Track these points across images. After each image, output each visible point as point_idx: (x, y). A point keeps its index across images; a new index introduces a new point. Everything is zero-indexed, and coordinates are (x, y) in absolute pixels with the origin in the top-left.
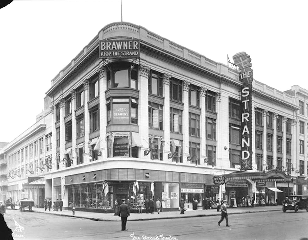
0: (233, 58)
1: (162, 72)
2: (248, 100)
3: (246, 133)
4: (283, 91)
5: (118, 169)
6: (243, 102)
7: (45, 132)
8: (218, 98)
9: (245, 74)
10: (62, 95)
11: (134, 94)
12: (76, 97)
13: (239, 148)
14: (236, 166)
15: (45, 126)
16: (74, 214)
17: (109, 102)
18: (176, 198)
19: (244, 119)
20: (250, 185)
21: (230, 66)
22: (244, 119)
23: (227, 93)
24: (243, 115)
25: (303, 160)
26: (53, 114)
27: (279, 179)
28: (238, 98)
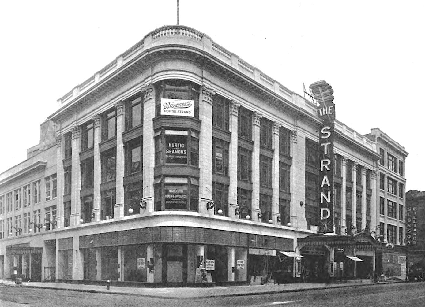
0: (310, 88)
1: (229, 99)
2: (330, 143)
3: (325, 185)
4: (362, 134)
5: (171, 228)
6: (322, 145)
7: (44, 173)
8: (293, 138)
9: (325, 109)
10: (77, 120)
11: (194, 126)
12: (100, 125)
13: (316, 204)
14: (312, 227)
15: (45, 165)
16: (108, 289)
17: (159, 133)
18: (243, 267)
19: (324, 167)
20: (328, 252)
21: (307, 97)
22: (324, 167)
23: (303, 133)
24: (322, 162)
25: (384, 222)
26: (60, 148)
27: (360, 246)
28: (316, 140)
